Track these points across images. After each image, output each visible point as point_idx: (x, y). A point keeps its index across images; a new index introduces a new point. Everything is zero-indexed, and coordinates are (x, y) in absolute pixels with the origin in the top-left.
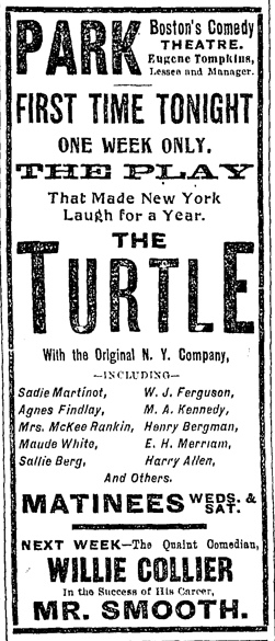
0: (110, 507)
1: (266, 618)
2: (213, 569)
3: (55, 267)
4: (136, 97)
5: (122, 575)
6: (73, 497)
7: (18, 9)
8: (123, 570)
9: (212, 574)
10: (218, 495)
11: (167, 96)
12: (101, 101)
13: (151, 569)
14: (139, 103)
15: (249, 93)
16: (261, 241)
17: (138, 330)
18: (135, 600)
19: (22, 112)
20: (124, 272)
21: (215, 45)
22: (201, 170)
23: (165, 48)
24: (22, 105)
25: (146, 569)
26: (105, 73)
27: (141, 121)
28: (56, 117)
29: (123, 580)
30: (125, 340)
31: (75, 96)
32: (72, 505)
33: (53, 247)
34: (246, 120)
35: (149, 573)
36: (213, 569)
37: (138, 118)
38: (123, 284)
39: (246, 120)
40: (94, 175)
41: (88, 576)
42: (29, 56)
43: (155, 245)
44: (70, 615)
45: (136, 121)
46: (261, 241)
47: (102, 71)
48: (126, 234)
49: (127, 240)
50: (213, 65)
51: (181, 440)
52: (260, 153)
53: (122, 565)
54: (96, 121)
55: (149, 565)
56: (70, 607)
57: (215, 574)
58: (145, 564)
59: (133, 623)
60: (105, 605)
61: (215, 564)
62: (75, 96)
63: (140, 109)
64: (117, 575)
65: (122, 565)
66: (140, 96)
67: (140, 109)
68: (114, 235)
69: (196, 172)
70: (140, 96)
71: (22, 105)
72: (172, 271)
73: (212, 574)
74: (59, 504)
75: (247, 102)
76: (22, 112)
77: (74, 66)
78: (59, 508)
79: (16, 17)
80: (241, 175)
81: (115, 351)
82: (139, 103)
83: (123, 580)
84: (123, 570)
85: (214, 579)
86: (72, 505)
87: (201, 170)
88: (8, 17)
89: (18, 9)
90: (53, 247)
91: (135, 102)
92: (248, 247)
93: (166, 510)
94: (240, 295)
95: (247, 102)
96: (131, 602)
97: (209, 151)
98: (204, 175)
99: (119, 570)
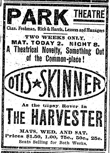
0: (71, 44)
1: (105, 145)
2: (86, 14)
3: (12, 113)
4: (22, 113)
6: (23, 41)
9: (103, 16)
12: (78, 12)
14: (23, 115)
17: (70, 117)
19: (88, 86)
20: (51, 112)
23: (33, 44)
24: (88, 82)
27: (24, 123)
28: (48, 57)
33: (12, 109)
36: (86, 14)
37: (23, 121)
38: (51, 115)
51: (92, 139)
56: (45, 14)
63: (24, 118)
66: (24, 113)
67: (24, 118)
70: (24, 113)
71: (88, 82)
72: (95, 12)
73: (103, 16)
74: (29, 17)
76: (88, 86)
78: (20, 43)
80: (60, 21)
82: (23, 115)
88: (5, 7)
90: (12, 109)
97: (87, 134)
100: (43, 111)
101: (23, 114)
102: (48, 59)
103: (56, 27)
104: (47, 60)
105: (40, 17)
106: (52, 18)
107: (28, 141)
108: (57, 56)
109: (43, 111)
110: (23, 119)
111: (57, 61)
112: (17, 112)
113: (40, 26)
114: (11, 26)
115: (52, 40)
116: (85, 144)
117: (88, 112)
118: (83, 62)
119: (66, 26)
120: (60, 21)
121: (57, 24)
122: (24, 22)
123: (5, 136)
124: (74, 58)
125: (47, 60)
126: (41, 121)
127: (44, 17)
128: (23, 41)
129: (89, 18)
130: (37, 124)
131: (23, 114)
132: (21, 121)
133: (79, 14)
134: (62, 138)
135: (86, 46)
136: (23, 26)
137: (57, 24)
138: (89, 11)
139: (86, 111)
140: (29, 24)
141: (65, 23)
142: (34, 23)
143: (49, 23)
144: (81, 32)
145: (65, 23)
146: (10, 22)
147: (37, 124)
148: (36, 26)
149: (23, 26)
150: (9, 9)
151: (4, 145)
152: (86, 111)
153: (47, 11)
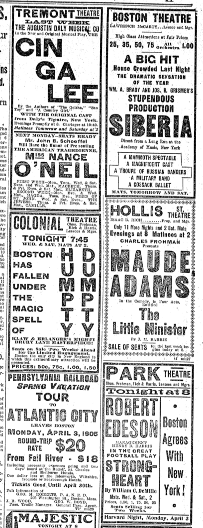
5: (189, 20)
7: (107, 364)
8: (190, 19)
10: (27, 431)
15: (168, 469)
16: (101, 84)
18: (30, 152)
21: (123, 456)
25: (95, 29)
31: (178, 57)
34: (114, 323)
39: (114, 323)
44: (26, 15)
46: (101, 84)
48: (18, 296)
49: (18, 298)
52: (99, 335)
53: (189, 17)
54: (166, 494)
59: (158, 155)
60: (19, 384)
62: (178, 57)
65: (189, 17)
68: (23, 236)
73: (189, 376)
75: (154, 404)
79: (106, 366)
80: (153, 377)
81: (184, 68)
84: (190, 19)
89: (107, 364)
92: (95, 87)
93: (76, 450)
95: (154, 404)
96: (40, 39)
99: (188, 19)
100: (51, 420)
103: (150, 382)
105: (136, 374)
106: (146, 375)
108: (74, 230)
109: (51, 420)
113: (135, 381)
114: (110, 381)
115: (53, 148)
116: (115, 502)
118: (183, 494)
119: (158, 381)
121: (58, 40)
122: (121, 378)
123: (104, 502)
124: (164, 418)
129: (177, 378)
133: (169, 374)
134: (13, 485)
136: (121, 381)
137: (58, 40)
138: (177, 372)
140: (126, 380)
141: (157, 379)
142: (130, 379)
144: (123, 28)
145: (157, 379)
146: (108, 378)
148: (131, 382)
149: (121, 381)
150: (107, 367)
153: (28, 10)
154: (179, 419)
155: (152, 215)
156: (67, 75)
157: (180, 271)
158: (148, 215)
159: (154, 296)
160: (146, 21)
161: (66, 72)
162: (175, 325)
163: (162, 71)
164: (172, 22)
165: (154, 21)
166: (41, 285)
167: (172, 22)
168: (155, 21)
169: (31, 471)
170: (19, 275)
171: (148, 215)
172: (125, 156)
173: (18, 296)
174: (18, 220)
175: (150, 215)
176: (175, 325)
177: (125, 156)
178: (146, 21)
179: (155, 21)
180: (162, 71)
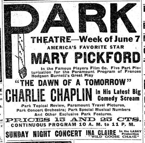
2: (73, 133)
5: (115, 134)
6: (55, 37)
8: (115, 133)
9: (73, 135)
11: (88, 80)
13: (70, 133)
14: (43, 92)
19: (73, 96)
22: (74, 119)
26: (62, 101)
29: (44, 101)
30: (89, 130)
32: (54, 39)
35: (70, 134)
36: (73, 133)
40: (38, 121)
41: (80, 98)
42: (73, 96)
43: (135, 137)
45: (42, 101)
47: (62, 100)
50: (114, 107)
55: (70, 132)
57: (74, 134)
58: (69, 132)
61: (74, 132)
63: (44, 95)
64: (31, 84)
65: (115, 132)
66: (44, 90)
67: (44, 95)
68: (31, 38)
69: (73, 119)
70: (44, 90)
73: (73, 135)
77: (55, 81)
80: (120, 21)
82: (43, 92)
83: (44, 101)
85: (73, 136)
86: (54, 39)
87: (74, 119)
91: (41, 92)
94: (110, 59)
98: (75, 120)
101: (43, 91)
102: (55, 97)
104: (54, 98)
107: (59, 109)
110: (43, 97)
111: (106, 100)
112: (39, 101)
117: (25, 81)
120: (120, 21)
125: (54, 98)
126: (20, 98)
127: (90, 18)
128: (55, 37)
130: (17, 101)
131: (43, 91)
132: (41, 98)
135: (42, 111)
139: (24, 81)
143: (103, 28)
147: (17, 101)
151: (13, 13)
152: (24, 81)
154: (122, 90)
155: (39, 101)
156: (58, 24)
157: (132, 93)
158: (36, 101)
159: (26, 101)
160: (58, 85)
161: (57, 18)
162: (121, 90)
163: (115, 93)
164: (45, 85)
165: (86, 84)
166: (61, 37)
167: (45, 85)
168: (87, 84)
169: (35, 112)
170: (83, 47)
171: (36, 101)
172: (78, 80)
173: (58, 37)
174: (55, 93)
175: (37, 101)
176: (121, 90)
177: (78, 80)
178: (58, 85)
179: (87, 84)
180: (115, 93)
